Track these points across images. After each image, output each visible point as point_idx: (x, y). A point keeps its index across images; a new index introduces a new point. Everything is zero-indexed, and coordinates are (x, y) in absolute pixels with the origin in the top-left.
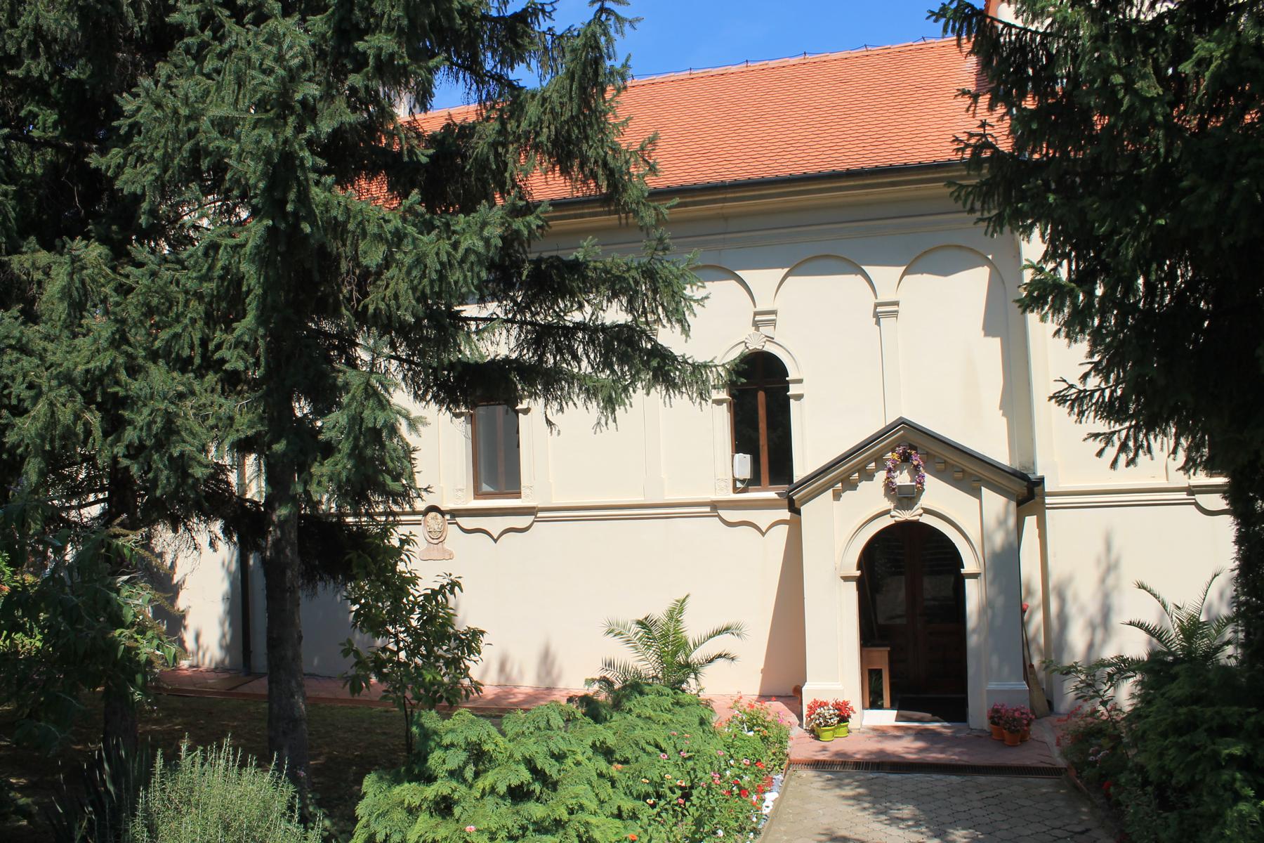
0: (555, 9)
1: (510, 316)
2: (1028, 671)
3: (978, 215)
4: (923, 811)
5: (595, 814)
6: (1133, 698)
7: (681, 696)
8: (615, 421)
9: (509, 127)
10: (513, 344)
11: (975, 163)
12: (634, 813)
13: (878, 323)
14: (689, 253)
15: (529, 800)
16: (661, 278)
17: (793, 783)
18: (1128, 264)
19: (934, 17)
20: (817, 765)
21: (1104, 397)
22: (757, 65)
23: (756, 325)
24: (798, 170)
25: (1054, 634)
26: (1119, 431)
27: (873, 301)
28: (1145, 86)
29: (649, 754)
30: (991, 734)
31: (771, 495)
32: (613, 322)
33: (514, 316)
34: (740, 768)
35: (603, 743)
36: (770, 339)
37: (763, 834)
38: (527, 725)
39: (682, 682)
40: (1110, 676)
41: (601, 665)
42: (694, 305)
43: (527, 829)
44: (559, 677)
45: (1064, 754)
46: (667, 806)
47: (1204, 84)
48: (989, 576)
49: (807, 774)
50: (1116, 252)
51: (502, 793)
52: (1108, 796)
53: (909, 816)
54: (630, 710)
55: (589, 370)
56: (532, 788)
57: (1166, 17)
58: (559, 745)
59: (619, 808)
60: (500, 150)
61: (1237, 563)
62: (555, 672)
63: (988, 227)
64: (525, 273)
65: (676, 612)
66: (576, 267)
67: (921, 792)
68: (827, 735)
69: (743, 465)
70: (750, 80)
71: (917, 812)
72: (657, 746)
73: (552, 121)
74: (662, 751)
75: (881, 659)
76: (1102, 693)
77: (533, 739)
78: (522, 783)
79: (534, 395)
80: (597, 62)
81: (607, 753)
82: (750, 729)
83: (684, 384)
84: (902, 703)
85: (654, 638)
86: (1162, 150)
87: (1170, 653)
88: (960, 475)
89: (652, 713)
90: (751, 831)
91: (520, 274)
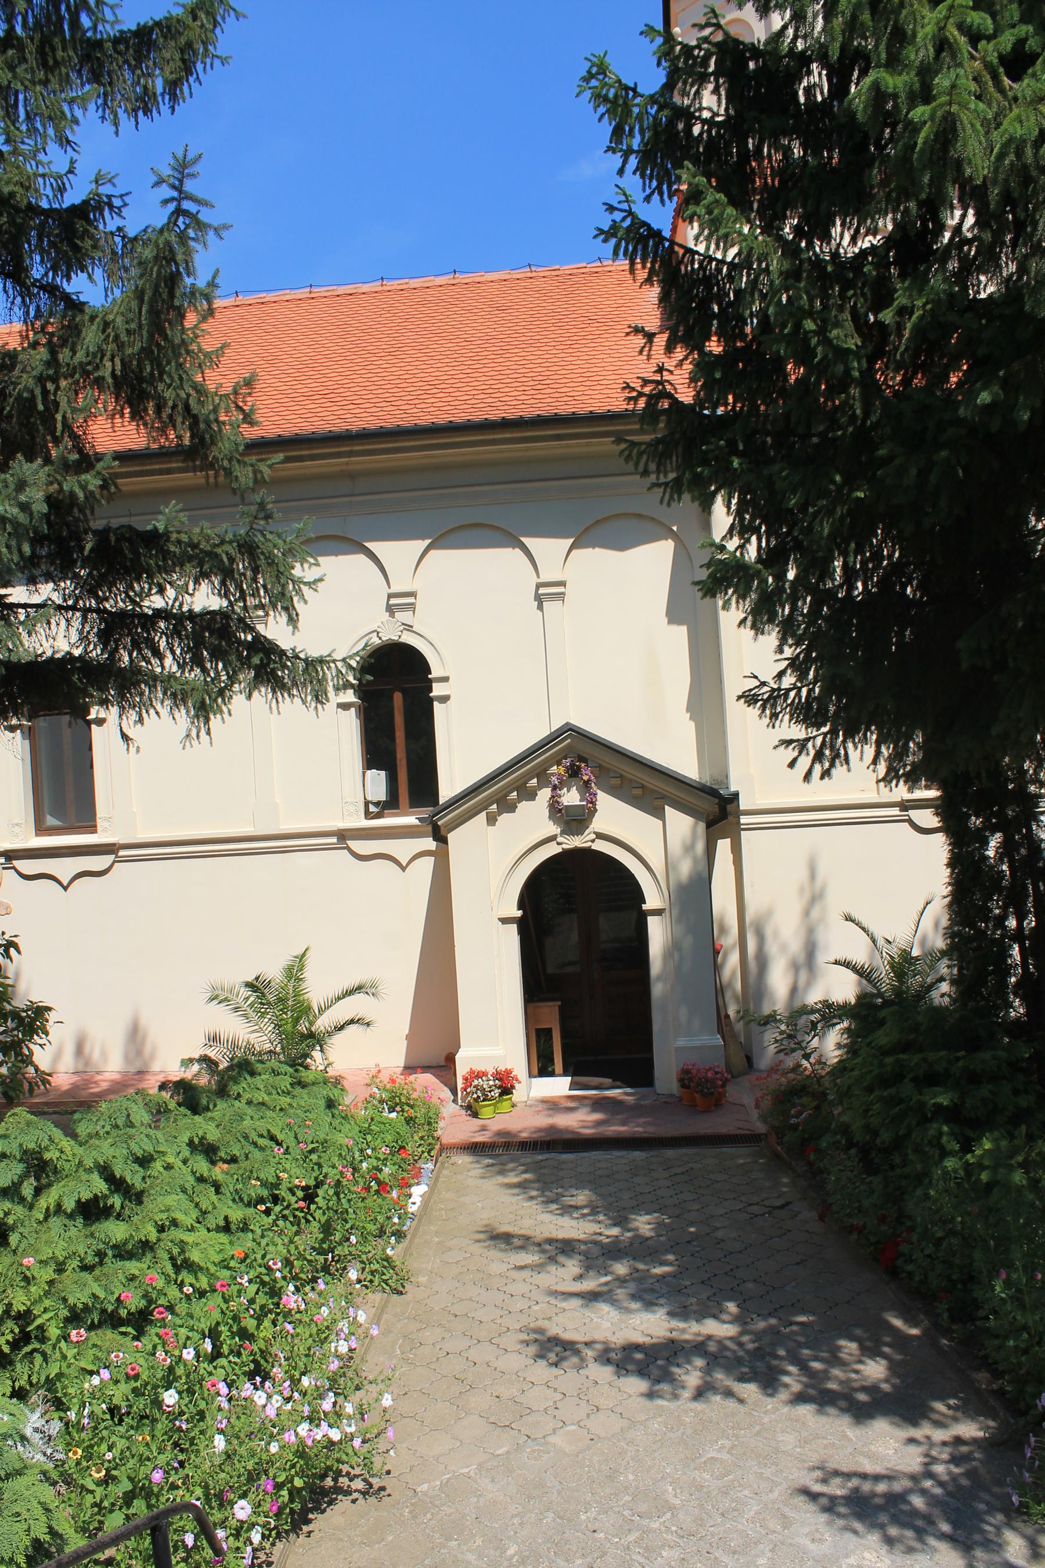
0: (125, 205)
1: (70, 603)
2: (722, 1022)
3: (653, 478)
4: (601, 1195)
5: (192, 1229)
6: (839, 1048)
7: (303, 1073)
8: (208, 733)
9: (61, 356)
10: (74, 637)
11: (651, 414)
12: (245, 1224)
13: (540, 607)
14: (298, 521)
15: (107, 1219)
16: (263, 553)
17: (445, 1172)
18: (823, 543)
19: (602, 237)
20: (475, 1149)
21: (800, 698)
22: (394, 284)
23: (391, 610)
24: (442, 418)
25: (752, 979)
26: (815, 737)
27: (534, 580)
28: (842, 334)
29: (262, 1149)
30: (681, 1099)
31: (411, 820)
32: (204, 609)
33: (76, 602)
34: (378, 1159)
35: (203, 1138)
36: (409, 628)
37: (409, 1237)
38: (102, 1123)
39: (306, 1056)
40: (814, 1025)
41: (203, 1041)
42: (305, 589)
43: (106, 1255)
44: (153, 1056)
45: (763, 1118)
46: (286, 1212)
47: (907, 334)
48: (675, 913)
49: (463, 1160)
50: (810, 529)
51: (69, 1211)
52: (810, 1164)
53: (584, 1203)
54: (239, 1095)
55: (175, 668)
56: (110, 1202)
57: (869, 254)
58: (142, 1145)
59: (226, 1218)
60: (50, 386)
61: (950, 888)
62: (147, 1051)
63: (664, 494)
64: (88, 547)
65: (295, 971)
66: (154, 539)
67: (599, 1172)
68: (487, 1112)
69: (377, 783)
70: (385, 303)
71: (594, 1198)
72: (273, 1138)
73: (116, 352)
74: (279, 1144)
75: (551, 1016)
76: (804, 1044)
77: (109, 1140)
78: (96, 1196)
79: (104, 703)
80: (173, 280)
81: (209, 1151)
82: (392, 1110)
83: (295, 684)
84: (573, 1068)
85: (268, 1004)
86: (858, 412)
87: (880, 995)
88: (639, 792)
89: (266, 1098)
90: (393, 1234)
91: (82, 549)
